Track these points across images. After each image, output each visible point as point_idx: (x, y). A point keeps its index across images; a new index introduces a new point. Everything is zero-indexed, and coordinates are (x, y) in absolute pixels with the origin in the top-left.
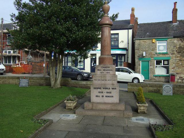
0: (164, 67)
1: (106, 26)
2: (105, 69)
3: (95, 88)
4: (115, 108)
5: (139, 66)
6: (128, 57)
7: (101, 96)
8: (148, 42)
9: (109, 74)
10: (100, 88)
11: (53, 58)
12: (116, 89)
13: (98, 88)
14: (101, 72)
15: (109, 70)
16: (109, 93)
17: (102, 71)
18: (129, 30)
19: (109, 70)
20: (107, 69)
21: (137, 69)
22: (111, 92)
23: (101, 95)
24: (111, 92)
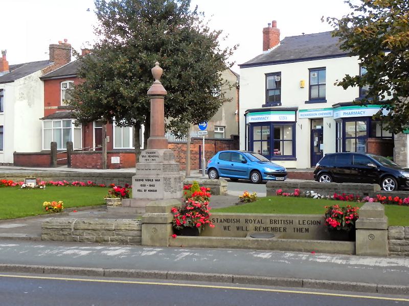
1: (157, 97)
3: (137, 180)
5: (402, 149)
7: (143, 191)
10: (142, 180)
13: (140, 180)
16: (152, 186)
17: (147, 158)
20: (152, 155)
21: (399, 157)
23: (143, 188)
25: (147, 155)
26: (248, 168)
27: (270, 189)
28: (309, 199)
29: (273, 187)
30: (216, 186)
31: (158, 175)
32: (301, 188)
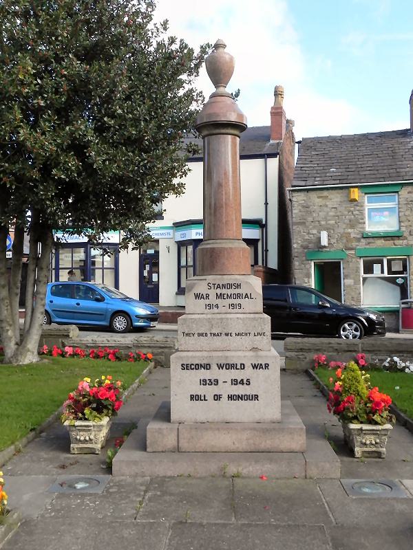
0: (384, 282)
2: (224, 291)
3: (186, 367)
4: (266, 443)
5: (306, 280)
6: (267, 251)
7: (210, 397)
8: (335, 198)
9: (240, 311)
10: (207, 367)
11: (9, 255)
12: (267, 366)
13: (198, 367)
14: (207, 302)
15: (238, 296)
16: (242, 382)
17: (213, 300)
18: (269, 160)
19: (238, 296)
20: (229, 292)
22: (248, 380)
23: (210, 391)
24: (248, 380)
25: (212, 293)
26: (107, 310)
27: (293, 354)
28: (394, 375)
29: (301, 350)
30: (166, 350)
31: (255, 349)
32: (363, 351)
